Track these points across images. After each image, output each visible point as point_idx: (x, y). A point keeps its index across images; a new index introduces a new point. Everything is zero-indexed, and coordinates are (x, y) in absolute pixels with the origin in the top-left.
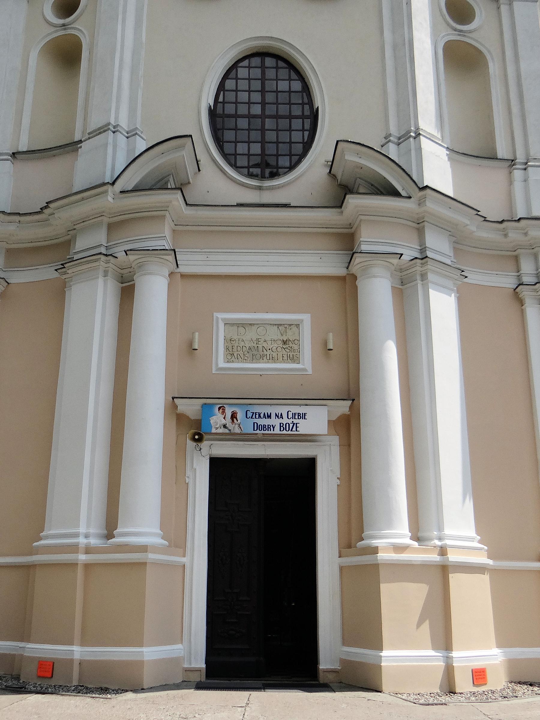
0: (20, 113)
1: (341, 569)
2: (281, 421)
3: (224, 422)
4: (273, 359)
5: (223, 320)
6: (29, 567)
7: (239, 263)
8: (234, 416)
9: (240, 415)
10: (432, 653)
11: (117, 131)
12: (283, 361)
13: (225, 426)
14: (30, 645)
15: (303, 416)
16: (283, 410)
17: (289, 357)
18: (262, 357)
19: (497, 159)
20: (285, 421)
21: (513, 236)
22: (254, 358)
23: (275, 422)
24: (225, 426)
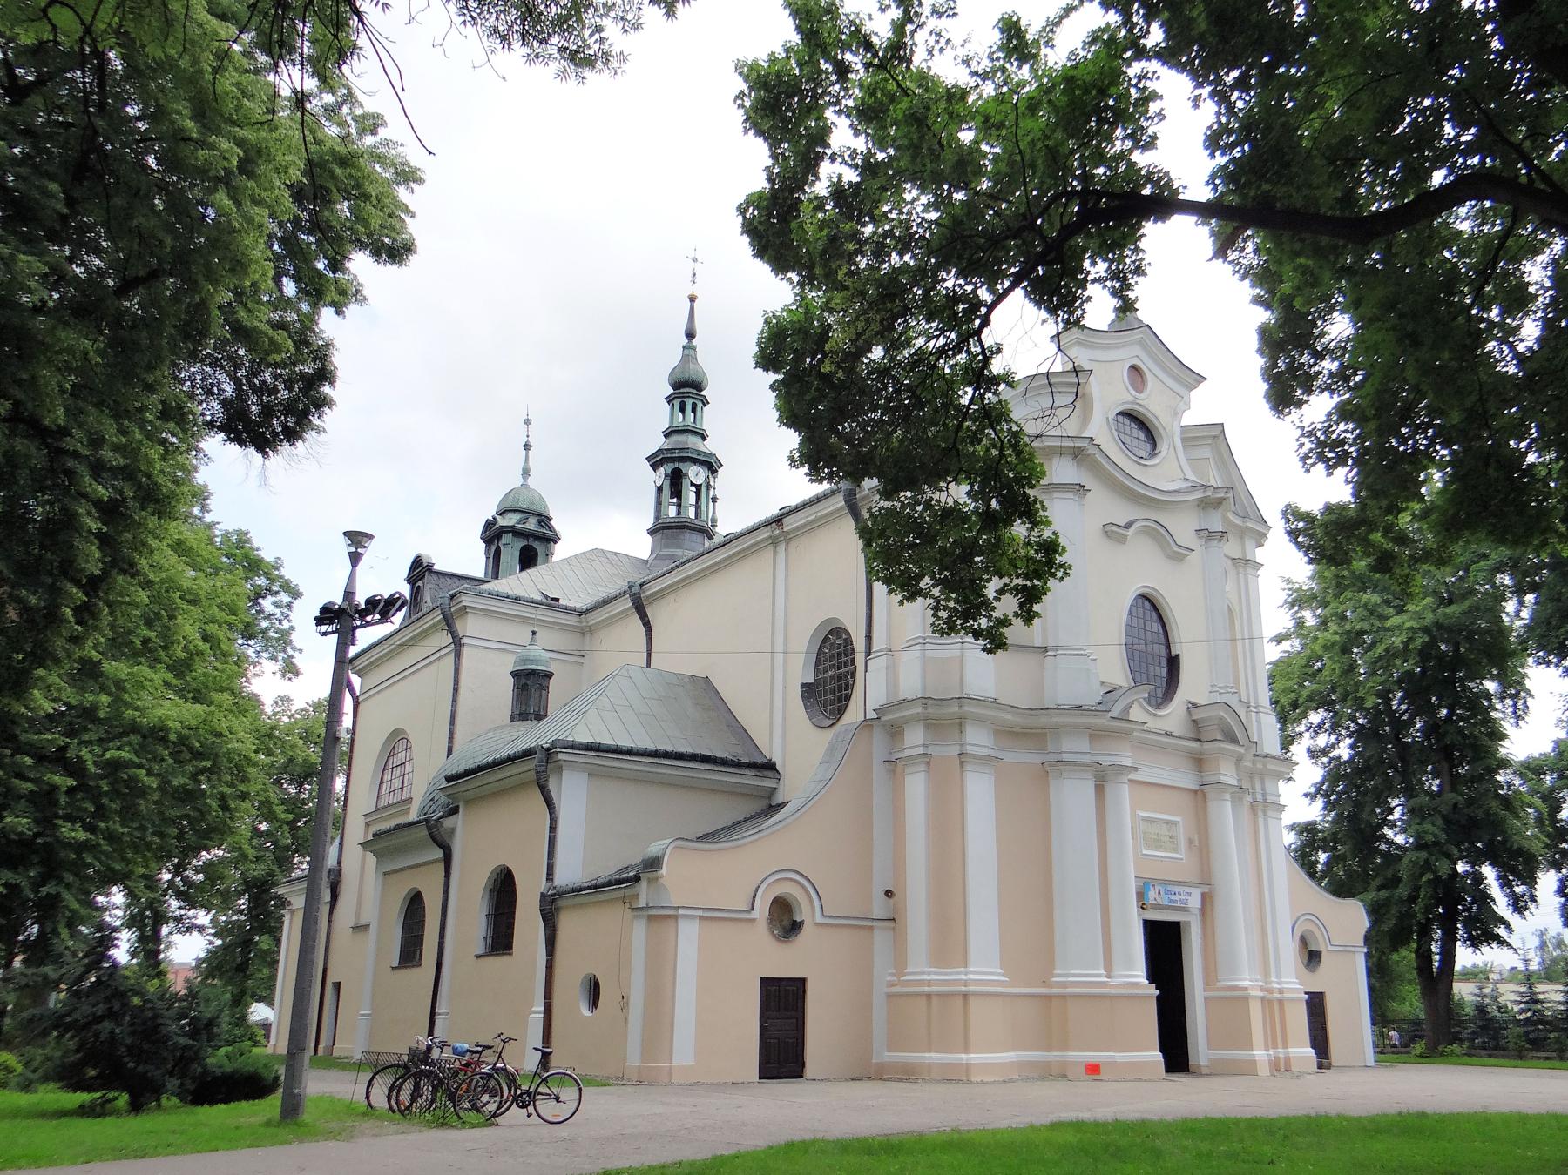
1: (1206, 999)
4: (1165, 850)
6: (1048, 997)
15: (1189, 894)
21: (1259, 766)
22: (1158, 848)
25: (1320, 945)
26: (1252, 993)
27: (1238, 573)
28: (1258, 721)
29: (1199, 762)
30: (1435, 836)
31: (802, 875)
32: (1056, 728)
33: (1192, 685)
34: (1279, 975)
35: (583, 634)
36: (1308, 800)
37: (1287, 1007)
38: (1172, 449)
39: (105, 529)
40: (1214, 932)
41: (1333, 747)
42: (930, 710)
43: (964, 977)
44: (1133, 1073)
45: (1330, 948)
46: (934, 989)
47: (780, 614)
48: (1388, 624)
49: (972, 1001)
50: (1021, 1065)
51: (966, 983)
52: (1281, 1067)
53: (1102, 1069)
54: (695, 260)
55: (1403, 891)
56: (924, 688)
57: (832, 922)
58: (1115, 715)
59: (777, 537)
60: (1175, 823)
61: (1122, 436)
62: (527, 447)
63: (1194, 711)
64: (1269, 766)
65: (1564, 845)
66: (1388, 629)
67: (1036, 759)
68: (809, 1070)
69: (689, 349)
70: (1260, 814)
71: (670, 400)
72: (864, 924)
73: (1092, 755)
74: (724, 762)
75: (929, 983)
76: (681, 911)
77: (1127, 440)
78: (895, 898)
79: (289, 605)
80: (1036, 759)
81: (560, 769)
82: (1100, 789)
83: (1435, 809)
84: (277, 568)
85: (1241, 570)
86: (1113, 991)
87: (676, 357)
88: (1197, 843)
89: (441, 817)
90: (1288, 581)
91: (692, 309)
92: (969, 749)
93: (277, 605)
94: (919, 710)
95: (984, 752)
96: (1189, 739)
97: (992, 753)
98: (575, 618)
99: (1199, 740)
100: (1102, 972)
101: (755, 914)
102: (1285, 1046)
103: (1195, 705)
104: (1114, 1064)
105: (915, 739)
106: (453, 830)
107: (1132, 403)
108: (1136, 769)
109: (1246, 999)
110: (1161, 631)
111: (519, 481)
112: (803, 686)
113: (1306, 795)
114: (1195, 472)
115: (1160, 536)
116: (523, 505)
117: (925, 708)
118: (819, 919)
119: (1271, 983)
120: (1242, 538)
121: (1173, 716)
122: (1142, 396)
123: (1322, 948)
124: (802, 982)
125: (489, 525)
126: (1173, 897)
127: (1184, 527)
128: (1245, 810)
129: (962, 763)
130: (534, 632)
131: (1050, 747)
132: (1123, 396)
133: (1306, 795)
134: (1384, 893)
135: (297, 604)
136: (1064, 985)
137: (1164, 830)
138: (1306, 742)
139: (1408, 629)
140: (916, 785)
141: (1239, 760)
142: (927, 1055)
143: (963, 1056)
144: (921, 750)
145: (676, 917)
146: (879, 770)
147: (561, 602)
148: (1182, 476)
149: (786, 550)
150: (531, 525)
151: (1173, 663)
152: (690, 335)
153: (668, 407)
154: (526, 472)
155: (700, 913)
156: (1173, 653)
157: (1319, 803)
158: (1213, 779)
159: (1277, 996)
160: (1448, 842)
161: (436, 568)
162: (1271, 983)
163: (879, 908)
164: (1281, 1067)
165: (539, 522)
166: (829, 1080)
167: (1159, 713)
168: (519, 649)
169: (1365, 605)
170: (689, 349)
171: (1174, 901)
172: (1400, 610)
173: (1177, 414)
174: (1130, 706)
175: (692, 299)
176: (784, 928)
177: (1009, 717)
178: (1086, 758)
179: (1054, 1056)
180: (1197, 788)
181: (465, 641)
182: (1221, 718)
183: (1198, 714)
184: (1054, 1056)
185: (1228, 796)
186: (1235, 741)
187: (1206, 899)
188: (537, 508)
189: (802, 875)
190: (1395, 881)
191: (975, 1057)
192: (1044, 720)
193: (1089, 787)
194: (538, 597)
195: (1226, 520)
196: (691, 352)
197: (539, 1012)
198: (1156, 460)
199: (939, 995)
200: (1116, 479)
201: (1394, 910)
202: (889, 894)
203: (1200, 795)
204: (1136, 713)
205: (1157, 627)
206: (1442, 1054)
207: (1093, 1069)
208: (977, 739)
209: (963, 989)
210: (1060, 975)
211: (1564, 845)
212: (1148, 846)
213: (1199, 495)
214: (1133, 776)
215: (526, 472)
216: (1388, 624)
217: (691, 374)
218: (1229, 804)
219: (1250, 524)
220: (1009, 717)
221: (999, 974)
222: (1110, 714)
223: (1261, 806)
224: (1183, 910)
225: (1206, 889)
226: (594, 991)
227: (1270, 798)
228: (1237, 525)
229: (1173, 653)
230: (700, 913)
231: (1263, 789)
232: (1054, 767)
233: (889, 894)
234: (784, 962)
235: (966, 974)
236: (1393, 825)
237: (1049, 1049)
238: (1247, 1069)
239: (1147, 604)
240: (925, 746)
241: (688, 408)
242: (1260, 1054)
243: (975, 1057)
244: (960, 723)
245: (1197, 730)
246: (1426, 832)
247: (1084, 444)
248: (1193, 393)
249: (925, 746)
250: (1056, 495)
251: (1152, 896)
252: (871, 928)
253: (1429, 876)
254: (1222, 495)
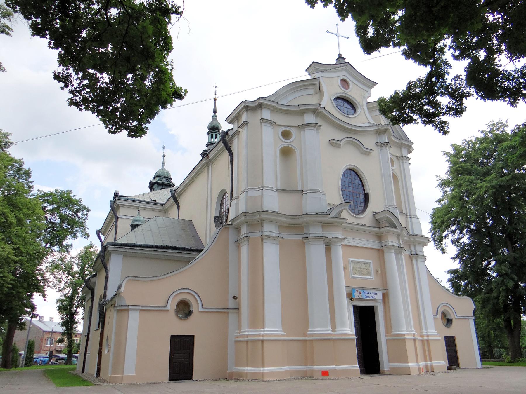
0: (276, 173)
1: (387, 340)
2: (371, 295)
3: (358, 295)
4: (364, 275)
5: (351, 260)
6: (305, 341)
7: (356, 242)
8: (360, 293)
9: (361, 293)
10: (444, 362)
11: (412, 217)
12: (367, 275)
13: (358, 296)
14: (315, 366)
15: (376, 294)
16: (371, 291)
17: (368, 274)
18: (362, 273)
19: (403, 213)
20: (372, 295)
21: (412, 239)
22: (360, 274)
24: (358, 296)
25: (452, 316)
26: (407, 337)
27: (399, 162)
28: (411, 221)
29: (379, 237)
30: (505, 271)
31: (192, 290)
32: (307, 224)
33: (374, 205)
34: (426, 329)
35: (165, 212)
36: (453, 261)
37: (431, 343)
38: (363, 111)
40: (389, 309)
41: (461, 238)
42: (248, 218)
43: (262, 333)
44: (345, 376)
45: (456, 317)
46: (249, 338)
47: (209, 191)
48: (477, 186)
49: (266, 344)
50: (291, 372)
51: (263, 335)
52: (430, 371)
53: (329, 374)
54: (216, 87)
55: (494, 294)
56: (247, 209)
57: (206, 310)
58: (333, 216)
59: (208, 163)
60: (369, 263)
61: (338, 106)
62: (164, 156)
63: (376, 215)
64: (416, 239)
66: (477, 188)
67: (299, 237)
68: (195, 377)
69: (215, 117)
70: (414, 260)
72: (224, 311)
73: (323, 234)
74: (184, 249)
75: (247, 336)
76: (130, 307)
77: (342, 108)
78: (238, 300)
79: (87, 214)
80: (299, 237)
81: (110, 254)
82: (328, 249)
83: (505, 260)
84: (80, 202)
85: (401, 161)
86: (334, 337)
87: (210, 119)
88: (379, 271)
89: (90, 278)
90: (438, 177)
92: (265, 233)
93: (83, 214)
94: (243, 218)
95: (274, 234)
96: (375, 227)
97: (278, 235)
98: (161, 207)
99: (379, 228)
100: (330, 329)
101: (168, 308)
102: (431, 360)
103: (376, 213)
104: (335, 371)
105: (244, 230)
106: (95, 283)
107: (343, 93)
108: (344, 239)
109: (404, 340)
110: (361, 184)
111: (161, 167)
112: (215, 217)
113: (452, 258)
114: (374, 120)
115: (357, 145)
116: (161, 174)
117: (246, 217)
118: (201, 309)
119: (423, 332)
120: (400, 148)
121: (366, 218)
122: (347, 91)
123: (452, 317)
124: (193, 336)
125: (151, 182)
126: (367, 295)
127: (369, 142)
128: (404, 259)
129: (262, 240)
130: (139, 211)
131: (305, 232)
132: (338, 90)
133: (452, 258)
134: (487, 295)
135: (89, 214)
136: (312, 335)
137: (363, 266)
138: (451, 237)
139: (486, 186)
140: (245, 250)
141: (398, 236)
142: (246, 368)
143: (261, 369)
144: (246, 235)
145: (128, 310)
146: (232, 246)
147: (157, 201)
148: (368, 122)
149: (212, 166)
150: (164, 181)
151: (366, 196)
152: (215, 112)
153: (208, 136)
154: (163, 164)
155: (140, 308)
156: (366, 192)
157: (458, 261)
158: (386, 244)
159: (425, 338)
160: (511, 273)
161: (119, 194)
162: (423, 332)
163: (231, 304)
164: (430, 371)
165: (167, 180)
166: (203, 380)
167: (359, 216)
168: (132, 218)
169: (468, 181)
170: (215, 117)
171: (367, 297)
172: (483, 181)
173: (365, 98)
174: (342, 211)
175: (215, 100)
176: (186, 314)
177: (285, 219)
178: (321, 235)
179: (308, 367)
180: (379, 248)
181: (119, 216)
182: (388, 218)
183: (378, 217)
184: (308, 367)
185: (393, 251)
186: (395, 227)
187: (385, 296)
188: (166, 175)
189: (192, 290)
190: (491, 291)
191: (266, 369)
192: (301, 220)
193: (321, 248)
194: (149, 201)
195: (389, 138)
196: (215, 117)
197: (88, 353)
198: (355, 115)
199: (252, 341)
200: (334, 122)
201: (491, 302)
202: (235, 297)
203: (381, 252)
204: (345, 214)
205: (358, 182)
206: (518, 361)
207: (325, 373)
208: (269, 229)
209: (261, 338)
210: (311, 331)
212: (354, 273)
213: (375, 128)
214: (344, 243)
215: (163, 164)
216: (477, 186)
217: (214, 124)
218: (393, 255)
219: (403, 142)
220: (285, 219)
221: (281, 331)
222: (330, 216)
223: (414, 256)
224: (375, 301)
225: (385, 291)
227: (418, 253)
228: (397, 143)
229: (366, 192)
230: (140, 308)
231: (415, 249)
232: (306, 240)
233: (235, 297)
234: (449, 333)
235: (264, 331)
236: (491, 269)
237: (306, 364)
238: (406, 372)
239: (352, 172)
240: (247, 233)
241: (214, 136)
242: (412, 365)
243: (266, 369)
244: (261, 223)
245: (378, 223)
246: (501, 270)
247: (316, 107)
248: (372, 90)
249: (247, 233)
250: (306, 129)
251: (356, 295)
252: (228, 313)
253: (504, 287)
254: (385, 127)
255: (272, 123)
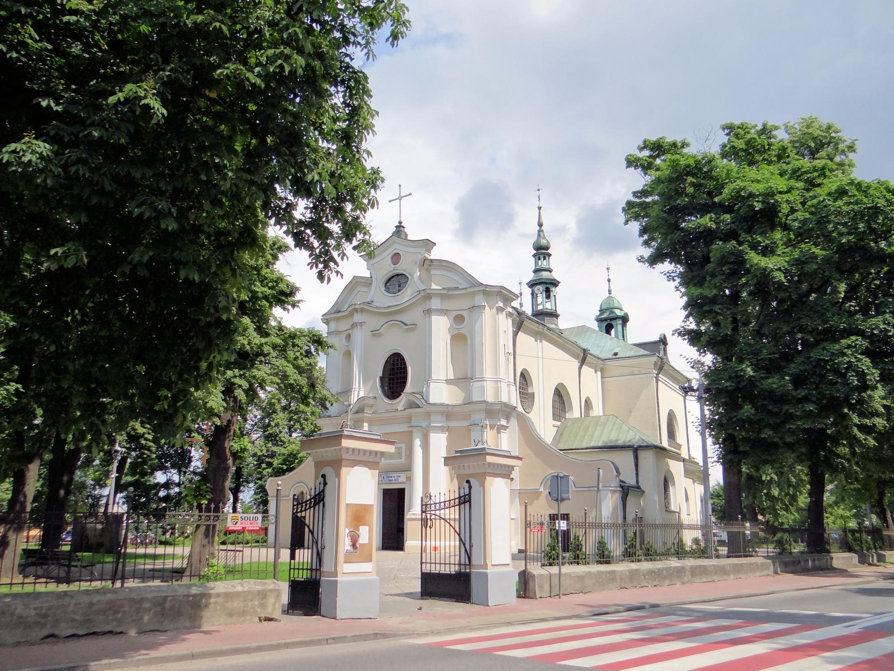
16: (395, 475)
23: (393, 478)
39: (35, 406)
62: (609, 280)
65: (3, 13)
71: (534, 256)
87: (535, 238)
91: (539, 213)
118: (574, 489)
152: (540, 225)
154: (610, 292)
175: (540, 208)
211: (3, 13)
215: (610, 292)
217: (543, 242)
226: (420, 609)
255: (444, 312)
